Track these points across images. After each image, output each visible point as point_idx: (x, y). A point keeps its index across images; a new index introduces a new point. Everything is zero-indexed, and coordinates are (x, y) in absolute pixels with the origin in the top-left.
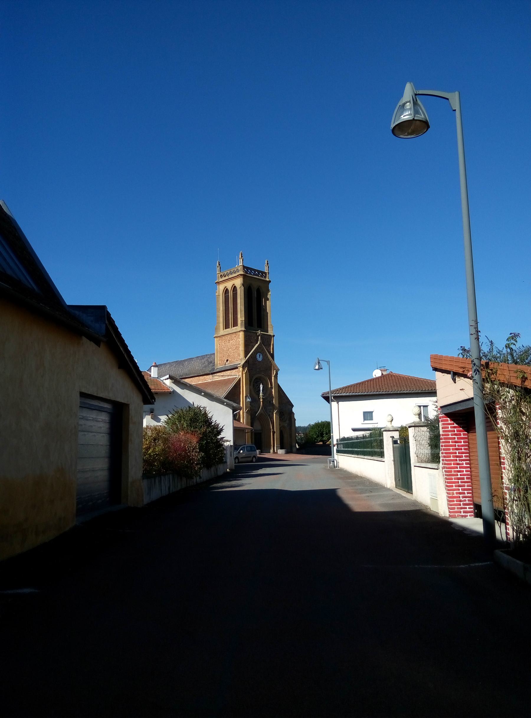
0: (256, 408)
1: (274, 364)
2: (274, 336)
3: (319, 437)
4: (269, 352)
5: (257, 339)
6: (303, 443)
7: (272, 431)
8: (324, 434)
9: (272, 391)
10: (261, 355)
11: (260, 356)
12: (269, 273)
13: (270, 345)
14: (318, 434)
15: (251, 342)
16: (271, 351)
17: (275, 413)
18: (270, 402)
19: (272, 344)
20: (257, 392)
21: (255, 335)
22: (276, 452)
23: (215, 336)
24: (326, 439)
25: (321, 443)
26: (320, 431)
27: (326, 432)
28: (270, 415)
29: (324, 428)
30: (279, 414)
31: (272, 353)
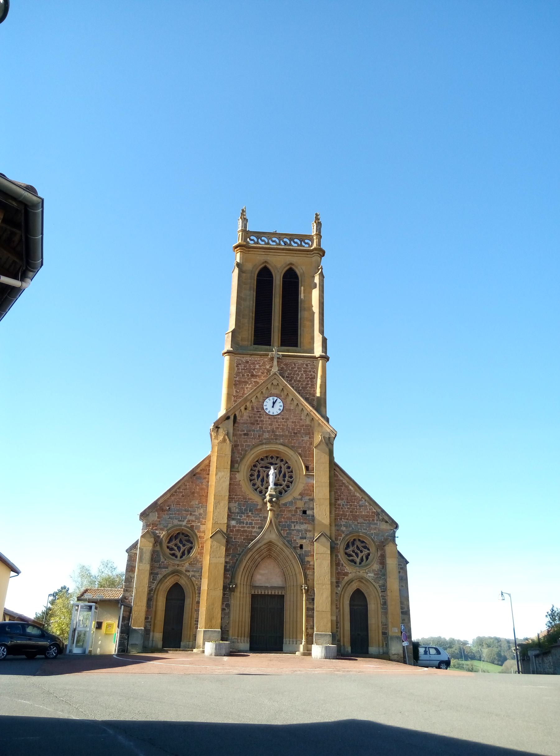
0: (253, 527)
15: (253, 376)
18: (304, 512)
28: (304, 547)
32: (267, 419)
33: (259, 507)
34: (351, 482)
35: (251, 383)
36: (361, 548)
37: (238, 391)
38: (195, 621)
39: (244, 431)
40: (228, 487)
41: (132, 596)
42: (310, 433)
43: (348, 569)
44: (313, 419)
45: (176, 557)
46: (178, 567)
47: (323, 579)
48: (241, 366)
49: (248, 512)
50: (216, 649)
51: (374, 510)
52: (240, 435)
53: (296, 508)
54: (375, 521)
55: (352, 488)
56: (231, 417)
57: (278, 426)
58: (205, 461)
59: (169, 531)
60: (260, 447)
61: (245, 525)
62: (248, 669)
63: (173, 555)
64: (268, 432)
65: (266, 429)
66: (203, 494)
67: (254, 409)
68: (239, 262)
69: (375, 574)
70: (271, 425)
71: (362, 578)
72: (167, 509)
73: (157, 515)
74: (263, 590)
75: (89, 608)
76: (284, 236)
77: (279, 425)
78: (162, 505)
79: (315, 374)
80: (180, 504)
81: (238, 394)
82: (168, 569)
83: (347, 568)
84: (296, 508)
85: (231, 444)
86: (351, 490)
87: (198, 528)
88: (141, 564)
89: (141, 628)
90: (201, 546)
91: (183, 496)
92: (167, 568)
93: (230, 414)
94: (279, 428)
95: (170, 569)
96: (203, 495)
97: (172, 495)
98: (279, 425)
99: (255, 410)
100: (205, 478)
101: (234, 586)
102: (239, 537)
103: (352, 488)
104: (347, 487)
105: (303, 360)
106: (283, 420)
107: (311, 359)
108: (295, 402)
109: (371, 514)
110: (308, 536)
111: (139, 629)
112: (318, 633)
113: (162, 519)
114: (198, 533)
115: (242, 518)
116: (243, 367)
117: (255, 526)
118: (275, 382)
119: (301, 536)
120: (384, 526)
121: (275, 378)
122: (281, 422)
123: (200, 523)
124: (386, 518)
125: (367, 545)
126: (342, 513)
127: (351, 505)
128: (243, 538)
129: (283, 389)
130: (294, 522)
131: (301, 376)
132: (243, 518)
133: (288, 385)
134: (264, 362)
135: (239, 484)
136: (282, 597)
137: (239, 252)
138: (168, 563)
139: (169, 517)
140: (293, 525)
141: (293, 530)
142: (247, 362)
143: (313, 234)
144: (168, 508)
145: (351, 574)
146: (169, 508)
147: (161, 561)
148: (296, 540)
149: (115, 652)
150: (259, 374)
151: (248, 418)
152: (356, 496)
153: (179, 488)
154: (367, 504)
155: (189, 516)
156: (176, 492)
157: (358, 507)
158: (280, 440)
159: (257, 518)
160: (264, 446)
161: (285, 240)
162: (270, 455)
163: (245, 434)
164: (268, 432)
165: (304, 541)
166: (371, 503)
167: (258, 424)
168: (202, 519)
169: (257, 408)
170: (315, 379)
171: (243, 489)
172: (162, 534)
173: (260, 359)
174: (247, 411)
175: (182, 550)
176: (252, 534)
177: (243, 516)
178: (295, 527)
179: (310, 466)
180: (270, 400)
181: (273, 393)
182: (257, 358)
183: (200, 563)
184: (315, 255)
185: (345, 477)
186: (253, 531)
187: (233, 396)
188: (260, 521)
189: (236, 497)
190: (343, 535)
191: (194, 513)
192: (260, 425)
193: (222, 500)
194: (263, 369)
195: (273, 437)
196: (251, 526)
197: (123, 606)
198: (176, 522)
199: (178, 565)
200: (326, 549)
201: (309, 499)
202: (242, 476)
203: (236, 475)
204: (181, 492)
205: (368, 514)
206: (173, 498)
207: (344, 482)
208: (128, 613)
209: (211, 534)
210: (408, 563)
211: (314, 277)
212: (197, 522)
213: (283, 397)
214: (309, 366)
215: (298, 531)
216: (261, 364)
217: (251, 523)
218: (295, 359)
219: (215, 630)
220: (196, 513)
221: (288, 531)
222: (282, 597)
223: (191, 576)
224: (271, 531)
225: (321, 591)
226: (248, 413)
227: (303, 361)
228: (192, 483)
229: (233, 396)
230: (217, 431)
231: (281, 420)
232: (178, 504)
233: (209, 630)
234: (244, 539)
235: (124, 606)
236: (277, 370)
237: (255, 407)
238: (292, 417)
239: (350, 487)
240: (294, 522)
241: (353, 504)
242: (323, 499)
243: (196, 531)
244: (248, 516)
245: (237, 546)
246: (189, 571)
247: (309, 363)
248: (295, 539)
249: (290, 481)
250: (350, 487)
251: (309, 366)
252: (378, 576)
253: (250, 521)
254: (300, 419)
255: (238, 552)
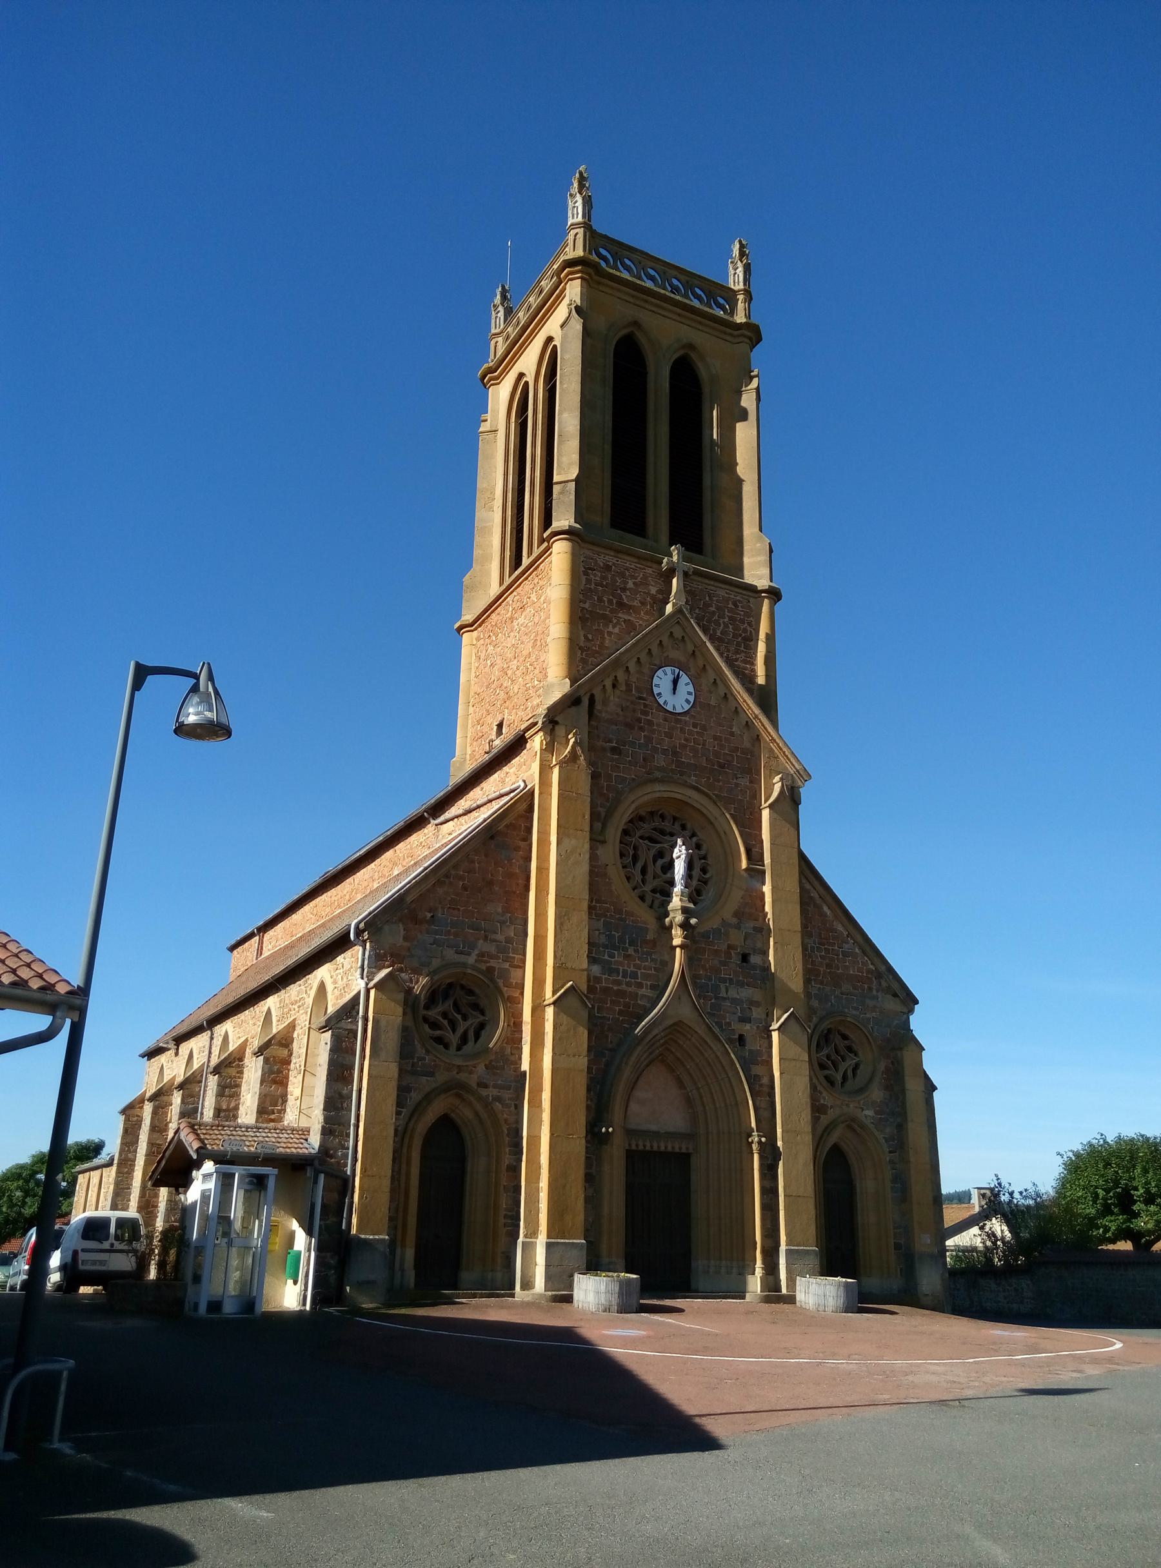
0: (640, 985)
1: (773, 740)
2: (774, 594)
3: (1112, 1213)
4: (747, 680)
5: (661, 596)
6: (60, 1202)
7: (755, 1147)
8: (1135, 1202)
9: (763, 894)
10: (684, 679)
11: (675, 682)
12: (748, 293)
13: (750, 641)
14: (1104, 1199)
15: (621, 605)
16: (754, 671)
17: (775, 1026)
18: (745, 958)
19: (762, 636)
20: (654, 891)
21: (649, 571)
22: (784, 1291)
23: (456, 626)
24: (1150, 1226)
25: (1126, 1246)
26: (1116, 1183)
27: (1147, 1191)
28: (748, 1040)
29: (1134, 1167)
30: (804, 1039)
31: (761, 680)
32: (661, 721)
33: (650, 936)
34: (829, 899)
35: (618, 623)
36: (843, 1051)
37: (590, 638)
38: (504, 1217)
39: (610, 741)
40: (587, 878)
41: (348, 1149)
42: (750, 769)
43: (827, 1098)
44: (758, 736)
45: (446, 1046)
46: (457, 1073)
47: (797, 1121)
48: (595, 575)
49: (627, 945)
50: (620, 1294)
51: (871, 967)
52: (604, 750)
53: (729, 947)
54: (874, 992)
55: (828, 912)
56: (583, 699)
57: (684, 742)
58: (519, 803)
59: (436, 978)
60: (648, 788)
61: (620, 978)
62: (845, 1365)
63: (439, 1040)
64: (664, 752)
65: (660, 744)
66: (514, 889)
67: (632, 691)
68: (579, 305)
69: (876, 1113)
70: (669, 735)
71: (854, 1120)
72: (428, 918)
73: (402, 932)
74: (648, 1141)
75: (255, 1180)
76: (675, 273)
77: (686, 740)
78: (414, 906)
79: (753, 631)
80: (459, 910)
81: (588, 644)
82: (432, 1079)
83: (825, 1094)
84: (729, 947)
85: (590, 769)
86: (825, 915)
87: (505, 974)
88: (376, 1063)
89: (381, 1237)
90: (514, 1023)
91: (465, 888)
92: (432, 1074)
93: (582, 693)
94: (686, 746)
95: (441, 1077)
96: (515, 893)
97: (439, 883)
98: (686, 740)
99: (634, 692)
100: (517, 849)
101: (610, 1130)
102: (608, 1005)
103: (828, 912)
104: (819, 908)
105: (728, 591)
106: (695, 730)
107: (744, 592)
108: (722, 690)
109: (865, 974)
110: (754, 1016)
111: (378, 1240)
112: (793, 1248)
113: (415, 943)
114: (506, 989)
115: (613, 960)
116: (597, 578)
117: (644, 982)
118: (678, 633)
119: (740, 1015)
120: (892, 1005)
121: (678, 622)
122: (691, 733)
123: (508, 964)
124: (895, 986)
125: (853, 1045)
126: (810, 966)
127: (827, 951)
128: (617, 1008)
129: (694, 651)
130: (724, 981)
131: (724, 628)
132: (616, 958)
133: (708, 644)
134: (645, 577)
135: (605, 874)
136: (685, 1158)
137: (578, 278)
138: (435, 1061)
139: (432, 941)
140: (722, 986)
141: (724, 999)
142: (608, 568)
143: (736, 288)
144: (429, 915)
145: (832, 1110)
146: (432, 916)
147: (417, 1055)
148: (729, 1024)
149: (304, 1304)
150: (635, 604)
151: (619, 710)
152: (835, 931)
153: (456, 867)
154: (857, 950)
155: (481, 941)
156: (447, 876)
157: (841, 956)
158: (690, 777)
159: (646, 963)
160: (657, 787)
161: (675, 282)
162: (658, 811)
163: (614, 750)
164: (664, 752)
165: (748, 1026)
166: (868, 949)
167: (642, 729)
168: (513, 954)
169: (638, 689)
170: (752, 643)
171: (613, 888)
172: (417, 982)
173: (637, 567)
174: (617, 692)
175: (460, 1030)
176: (637, 1001)
177: (616, 957)
178: (727, 994)
179: (753, 850)
180: (666, 674)
181: (670, 657)
182: (629, 563)
183: (512, 1066)
184: (742, 339)
185: (816, 884)
186: (640, 993)
187: (577, 647)
188: (653, 972)
189: (598, 905)
190: (814, 1019)
191: (494, 936)
192: (646, 733)
193: (574, 910)
194: (643, 592)
195: (674, 767)
196: (635, 982)
197: (322, 1176)
198: (450, 954)
199: (460, 1069)
200: (800, 1050)
201: (755, 929)
202: (609, 853)
203: (597, 849)
204: (461, 878)
205: (860, 974)
206: (440, 891)
207: (812, 895)
208: (336, 1196)
209: (553, 995)
210: (937, 1089)
211: (739, 394)
212: (500, 961)
213: (693, 671)
214: (740, 609)
215: (735, 1001)
216: (639, 579)
217: (634, 975)
218: (712, 583)
219: (573, 1243)
220: (500, 937)
221: (713, 1001)
222: (684, 1159)
223: (491, 1098)
224: (679, 998)
225: (794, 1147)
226: (619, 697)
227: (727, 593)
228: (486, 856)
229: (580, 649)
230: (553, 730)
231: (691, 728)
232: (454, 909)
233: (559, 1240)
234: (621, 1013)
235: (327, 1174)
236: (684, 603)
237: (634, 684)
238: (712, 725)
239: (825, 909)
240: (724, 981)
241: (831, 948)
242: (789, 930)
243: (500, 982)
244: (627, 957)
245: (606, 1029)
246: (486, 1086)
247: (739, 601)
248: (728, 1020)
249: (704, 880)
250: (825, 909)
251: (740, 609)
252: (883, 1116)
253: (632, 969)
254: (730, 732)
255: (610, 1046)
